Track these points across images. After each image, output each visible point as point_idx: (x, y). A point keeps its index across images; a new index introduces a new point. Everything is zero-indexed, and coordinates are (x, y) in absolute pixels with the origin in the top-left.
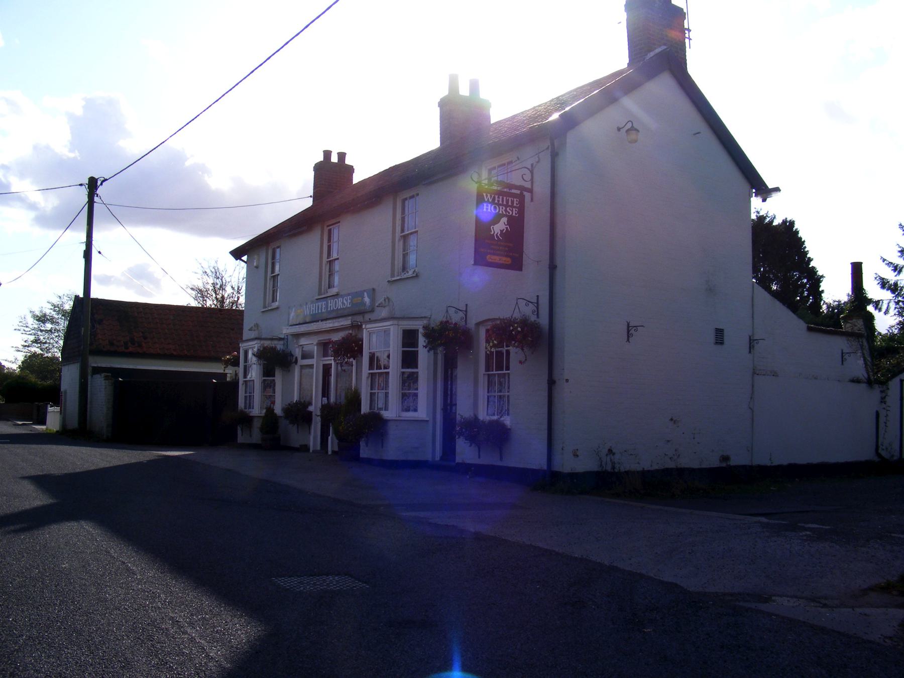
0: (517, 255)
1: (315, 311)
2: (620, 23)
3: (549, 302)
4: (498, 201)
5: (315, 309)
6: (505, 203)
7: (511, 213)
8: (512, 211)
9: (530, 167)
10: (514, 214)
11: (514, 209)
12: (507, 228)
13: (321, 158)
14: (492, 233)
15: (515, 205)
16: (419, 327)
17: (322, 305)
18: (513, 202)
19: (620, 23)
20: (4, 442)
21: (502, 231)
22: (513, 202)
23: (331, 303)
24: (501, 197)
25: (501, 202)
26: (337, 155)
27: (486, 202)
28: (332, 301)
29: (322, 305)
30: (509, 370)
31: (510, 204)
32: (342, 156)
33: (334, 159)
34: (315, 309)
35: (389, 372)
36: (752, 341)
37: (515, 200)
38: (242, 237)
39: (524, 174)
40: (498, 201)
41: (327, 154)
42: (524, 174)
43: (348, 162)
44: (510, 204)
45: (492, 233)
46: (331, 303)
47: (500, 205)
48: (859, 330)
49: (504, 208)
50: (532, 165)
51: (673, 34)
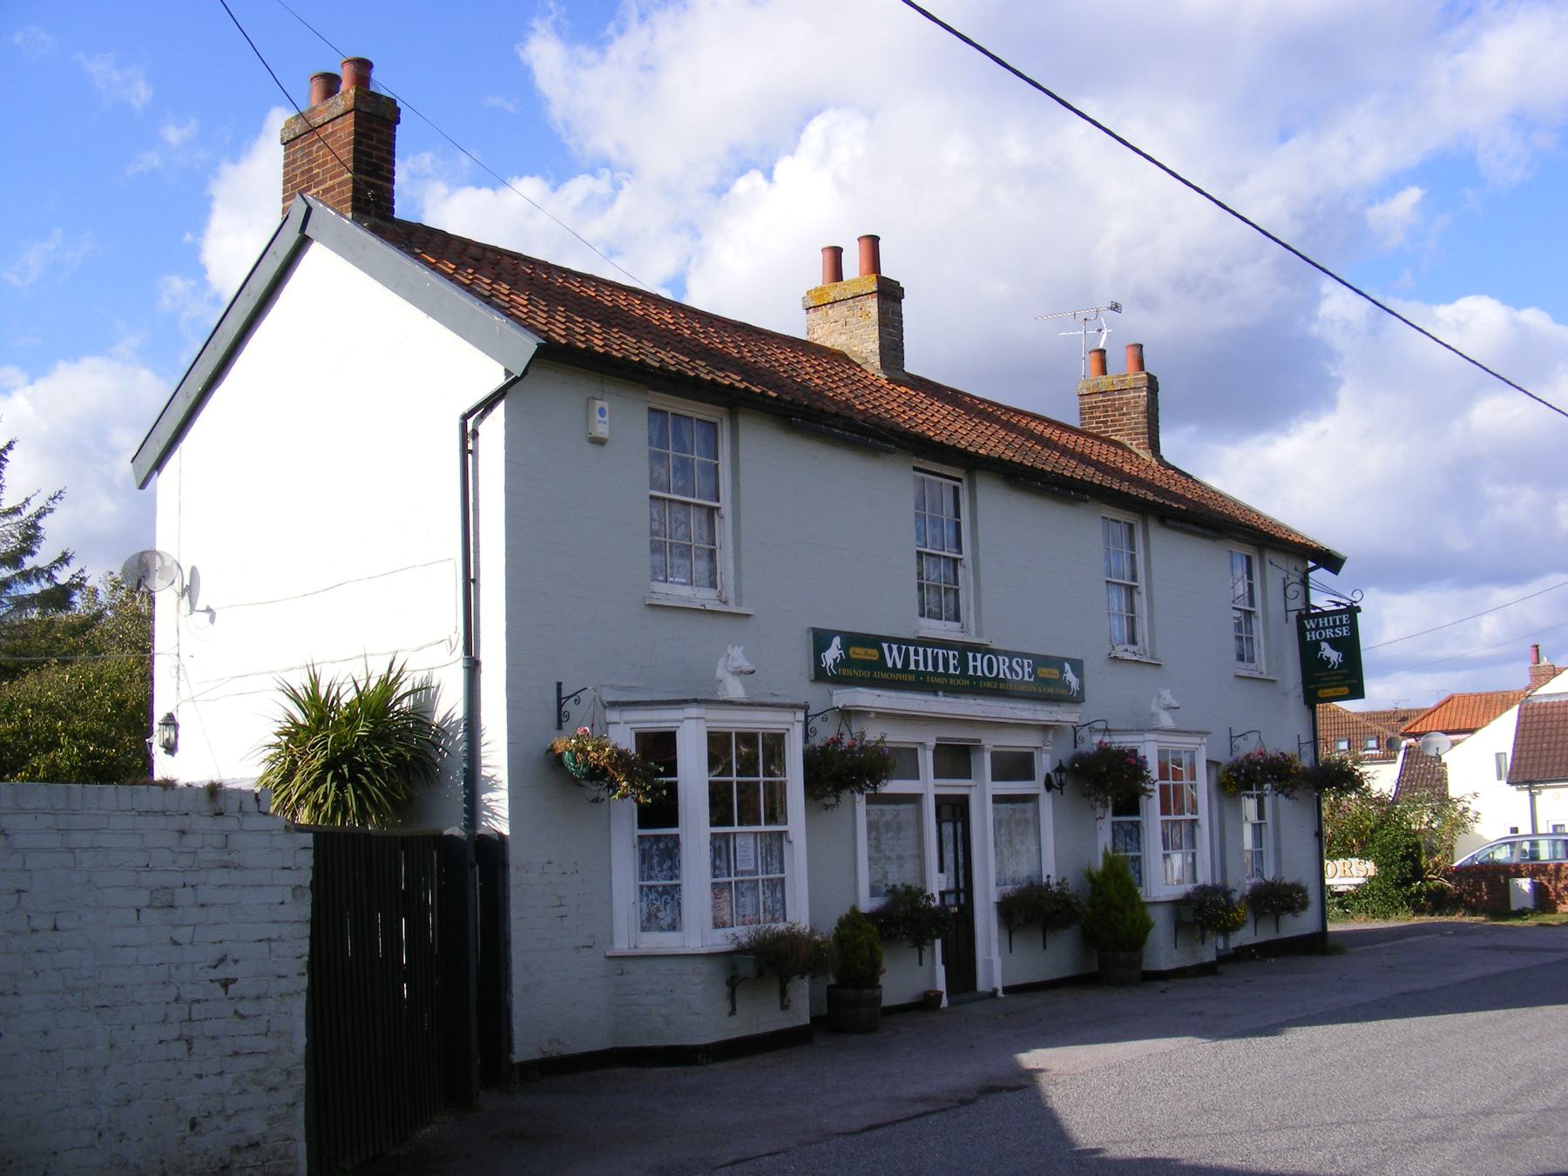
0: (1355, 681)
2: (192, 656)
4: (1323, 624)
6: (1331, 624)
7: (1341, 634)
8: (1342, 631)
10: (1345, 634)
11: (1344, 628)
12: (841, 654)
14: (824, 666)
15: (1345, 622)
16: (1138, 745)
18: (1341, 620)
19: (192, 656)
21: (835, 660)
22: (1341, 620)
24: (1326, 619)
25: (1326, 625)
27: (1308, 631)
31: (1338, 623)
36: (563, 701)
38: (1336, 711)
40: (1323, 624)
44: (1338, 623)
45: (824, 666)
47: (1327, 628)
48: (864, 421)
49: (1331, 630)
51: (132, 692)
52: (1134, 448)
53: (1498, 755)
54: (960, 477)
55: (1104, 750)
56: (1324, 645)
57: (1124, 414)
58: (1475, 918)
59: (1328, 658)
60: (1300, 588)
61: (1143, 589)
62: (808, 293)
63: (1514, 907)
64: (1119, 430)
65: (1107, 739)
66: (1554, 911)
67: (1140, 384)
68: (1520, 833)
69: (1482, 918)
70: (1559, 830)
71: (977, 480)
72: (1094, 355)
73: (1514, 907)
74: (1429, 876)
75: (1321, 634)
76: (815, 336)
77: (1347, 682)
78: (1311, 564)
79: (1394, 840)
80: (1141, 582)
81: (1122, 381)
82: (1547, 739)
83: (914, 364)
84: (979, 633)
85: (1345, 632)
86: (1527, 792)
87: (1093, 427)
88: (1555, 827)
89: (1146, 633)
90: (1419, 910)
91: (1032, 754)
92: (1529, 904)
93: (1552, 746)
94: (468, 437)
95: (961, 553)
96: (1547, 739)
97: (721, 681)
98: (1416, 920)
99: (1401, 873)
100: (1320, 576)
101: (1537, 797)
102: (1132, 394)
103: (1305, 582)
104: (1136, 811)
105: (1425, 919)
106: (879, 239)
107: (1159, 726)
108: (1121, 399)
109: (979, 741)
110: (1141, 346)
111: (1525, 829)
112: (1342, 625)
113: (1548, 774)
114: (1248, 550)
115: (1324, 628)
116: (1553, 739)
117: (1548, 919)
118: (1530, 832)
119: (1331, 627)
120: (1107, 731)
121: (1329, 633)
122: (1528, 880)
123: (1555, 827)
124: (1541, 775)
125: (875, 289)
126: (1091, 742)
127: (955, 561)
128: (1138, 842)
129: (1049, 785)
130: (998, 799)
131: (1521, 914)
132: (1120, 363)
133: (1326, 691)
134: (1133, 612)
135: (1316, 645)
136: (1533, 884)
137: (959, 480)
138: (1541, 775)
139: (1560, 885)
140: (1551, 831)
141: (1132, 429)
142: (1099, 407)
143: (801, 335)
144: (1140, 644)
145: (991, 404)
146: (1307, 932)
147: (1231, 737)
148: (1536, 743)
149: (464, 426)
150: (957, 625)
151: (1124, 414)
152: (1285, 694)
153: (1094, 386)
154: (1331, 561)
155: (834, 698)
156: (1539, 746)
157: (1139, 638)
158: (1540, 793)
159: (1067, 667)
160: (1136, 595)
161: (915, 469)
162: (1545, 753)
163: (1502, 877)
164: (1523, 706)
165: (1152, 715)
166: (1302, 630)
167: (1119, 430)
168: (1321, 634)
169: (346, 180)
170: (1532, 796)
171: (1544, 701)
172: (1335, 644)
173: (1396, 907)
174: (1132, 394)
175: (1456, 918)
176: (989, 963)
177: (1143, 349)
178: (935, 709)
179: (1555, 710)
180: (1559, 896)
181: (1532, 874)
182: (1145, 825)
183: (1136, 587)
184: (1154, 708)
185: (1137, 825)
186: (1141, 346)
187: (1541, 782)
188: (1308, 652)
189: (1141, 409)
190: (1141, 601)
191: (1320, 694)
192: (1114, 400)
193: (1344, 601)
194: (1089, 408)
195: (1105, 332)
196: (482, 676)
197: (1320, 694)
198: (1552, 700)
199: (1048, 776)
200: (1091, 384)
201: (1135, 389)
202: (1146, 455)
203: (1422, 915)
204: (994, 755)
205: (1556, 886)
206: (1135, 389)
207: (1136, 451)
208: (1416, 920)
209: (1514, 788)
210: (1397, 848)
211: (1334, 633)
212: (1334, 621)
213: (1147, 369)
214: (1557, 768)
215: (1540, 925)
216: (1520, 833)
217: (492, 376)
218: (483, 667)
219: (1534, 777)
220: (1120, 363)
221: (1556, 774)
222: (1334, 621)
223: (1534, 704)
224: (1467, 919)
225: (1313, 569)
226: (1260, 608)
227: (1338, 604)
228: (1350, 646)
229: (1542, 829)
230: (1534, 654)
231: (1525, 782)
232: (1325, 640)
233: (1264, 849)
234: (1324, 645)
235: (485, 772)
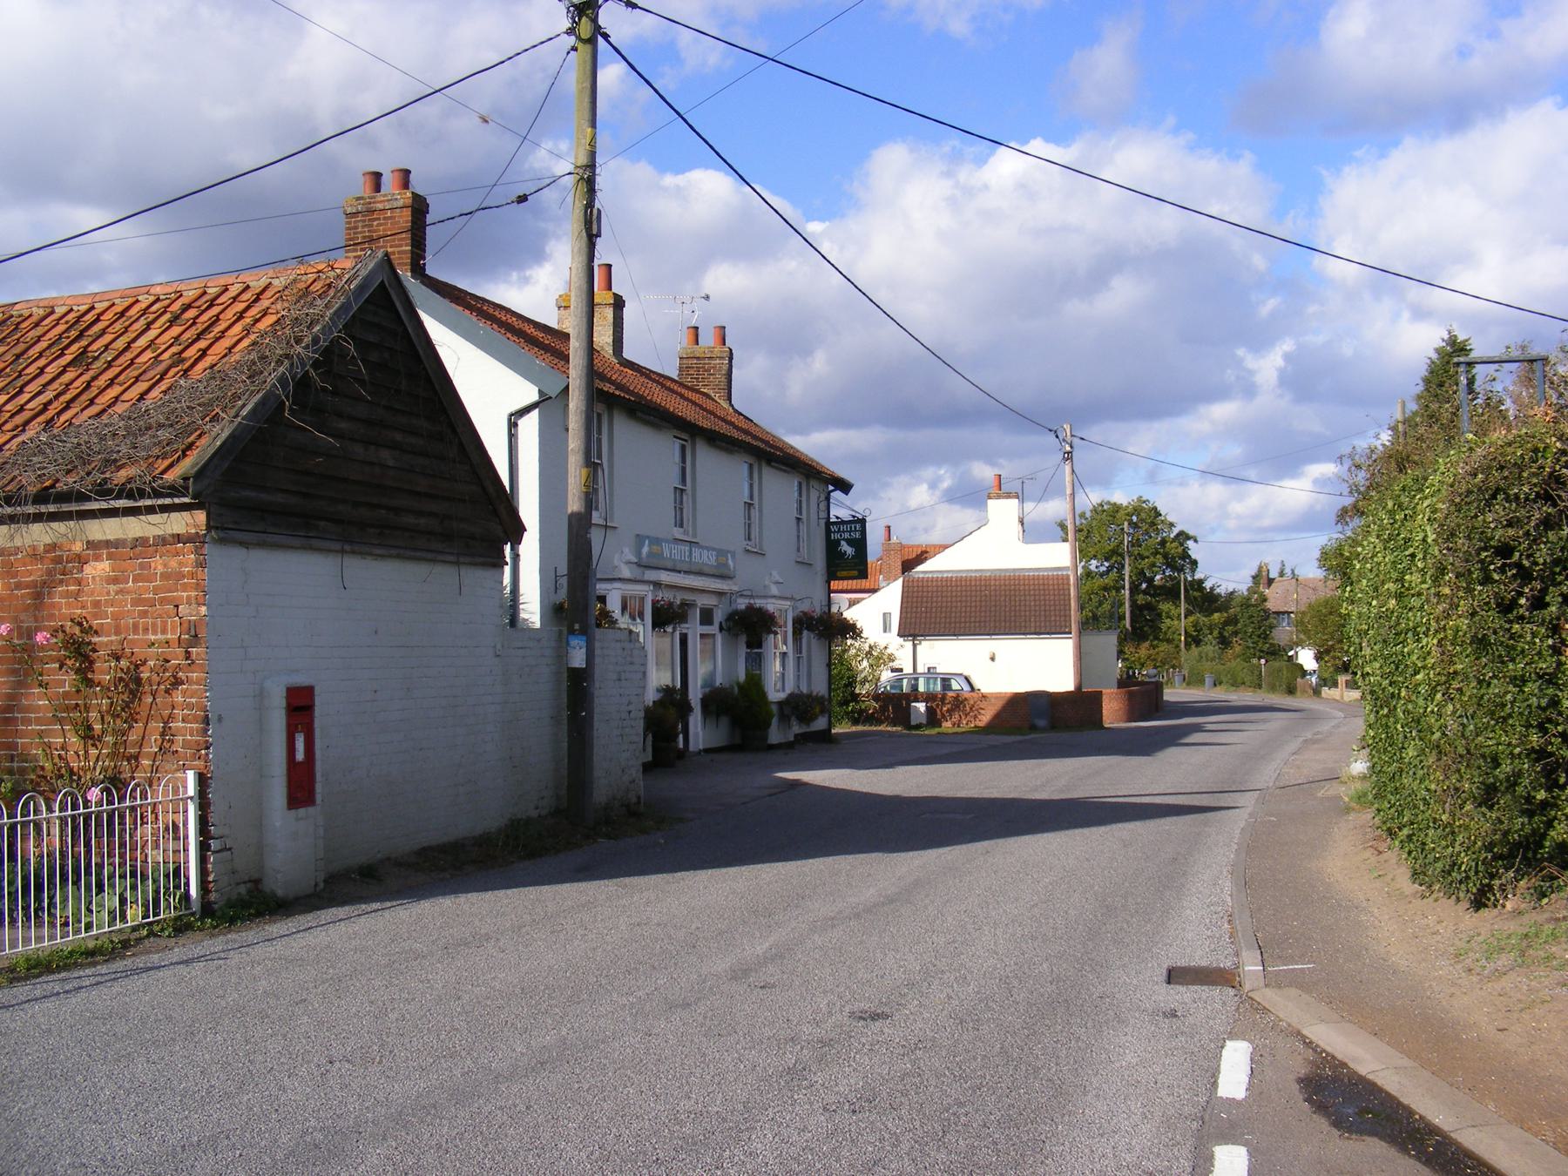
18: (855, 527)
22: (855, 527)
52: (716, 398)
53: (884, 614)
54: (686, 438)
55: (750, 608)
56: (843, 543)
57: (711, 374)
58: (894, 728)
59: (845, 552)
60: (825, 503)
61: (605, 465)
62: (560, 296)
63: (913, 723)
64: (707, 385)
65: (752, 601)
66: (941, 726)
67: (725, 355)
68: (905, 672)
69: (900, 729)
70: (932, 671)
71: (615, 412)
72: (691, 330)
73: (913, 723)
74: (863, 699)
75: (841, 536)
76: (564, 326)
77: (858, 567)
78: (831, 488)
79: (840, 673)
80: (756, 501)
81: (712, 352)
82: (925, 605)
83: (628, 354)
84: (695, 535)
85: (858, 535)
86: (911, 643)
87: (688, 381)
88: (929, 669)
89: (757, 534)
90: (856, 722)
91: (712, 609)
92: (924, 722)
93: (928, 610)
94: (512, 425)
95: (685, 486)
96: (925, 605)
97: (616, 567)
98: (854, 729)
99: (844, 696)
100: (837, 495)
101: (918, 647)
102: (718, 361)
103: (828, 499)
104: (760, 646)
105: (860, 728)
106: (410, 172)
107: (770, 594)
108: (710, 364)
109: (694, 601)
110: (724, 328)
111: (908, 669)
112: (856, 530)
113: (957, 630)
114: (751, 460)
115: (844, 532)
116: (929, 605)
117: (936, 730)
118: (912, 672)
119: (847, 531)
120: (751, 597)
121: (847, 535)
122: (924, 704)
123: (929, 669)
124: (922, 631)
125: (612, 302)
126: (742, 604)
127: (682, 490)
128: (760, 666)
129: (721, 629)
130: (702, 636)
131: (918, 727)
132: (708, 339)
133: (843, 573)
134: (749, 519)
135: (838, 542)
136: (927, 706)
137: (686, 441)
138: (922, 631)
139: (945, 709)
140: (926, 671)
141: (717, 385)
142: (693, 368)
143: (553, 324)
144: (753, 540)
145: (648, 370)
146: (821, 728)
147: (556, 576)
148: (917, 607)
149: (510, 420)
150: (681, 530)
151: (711, 374)
152: (816, 573)
153: (691, 353)
154: (845, 487)
155: (646, 576)
156: (919, 610)
157: (753, 537)
158: (920, 643)
159: (729, 555)
160: (801, 524)
161: (675, 437)
162: (924, 615)
163: (904, 702)
164: (906, 579)
165: (765, 586)
166: (828, 532)
167: (707, 385)
168: (841, 536)
169: (404, 252)
170: (915, 646)
171: (921, 576)
172: (850, 542)
173: (839, 720)
174: (718, 361)
175: (881, 728)
176: (696, 734)
177: (411, 176)
178: (687, 583)
179: (930, 584)
180: (943, 716)
181: (926, 701)
182: (765, 654)
183: (685, 490)
184: (616, 562)
185: (759, 655)
186: (724, 328)
187: (922, 636)
188: (832, 547)
189: (723, 372)
190: (755, 513)
191: (839, 574)
192: (705, 364)
193: (857, 515)
194: (686, 368)
195: (697, 313)
196: (520, 563)
197: (839, 574)
198: (927, 576)
199: (721, 623)
200: (689, 351)
201: (721, 358)
202: (725, 405)
203: (858, 725)
204: (701, 609)
205: (942, 709)
206: (721, 358)
207: (719, 401)
208: (854, 729)
209: (902, 639)
210: (842, 678)
211: (850, 535)
212: (851, 528)
213: (615, 289)
214: (932, 626)
215: (939, 733)
216: (905, 672)
217: (530, 394)
218: (521, 558)
219: (917, 632)
220: (708, 339)
221: (932, 630)
222: (851, 528)
223: (914, 578)
224: (889, 729)
225: (832, 491)
226: (690, 489)
227: (854, 517)
228: (860, 544)
229: (920, 669)
230: (887, 533)
231: (910, 636)
232: (844, 539)
233: (801, 673)
234: (843, 543)
235: (523, 615)
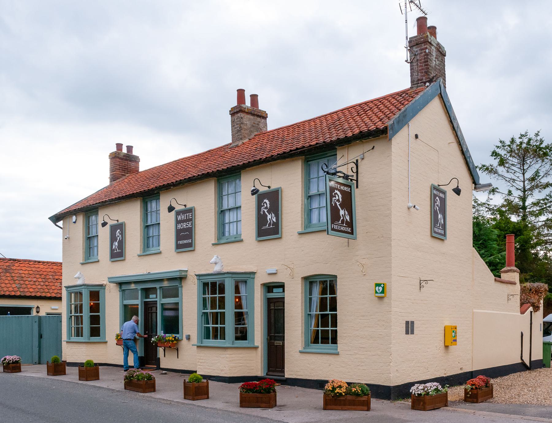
1: (185, 218)
3: (276, 288)
5: (185, 217)
9: (355, 161)
13: (114, 149)
17: (189, 215)
20: (328, 348)
23: (179, 225)
26: (126, 148)
28: (180, 224)
29: (189, 215)
30: (82, 325)
32: (130, 148)
33: (125, 150)
34: (185, 217)
35: (82, 316)
37: (338, 185)
39: (353, 167)
41: (119, 146)
42: (353, 167)
43: (135, 153)
46: (179, 225)
50: (357, 161)
